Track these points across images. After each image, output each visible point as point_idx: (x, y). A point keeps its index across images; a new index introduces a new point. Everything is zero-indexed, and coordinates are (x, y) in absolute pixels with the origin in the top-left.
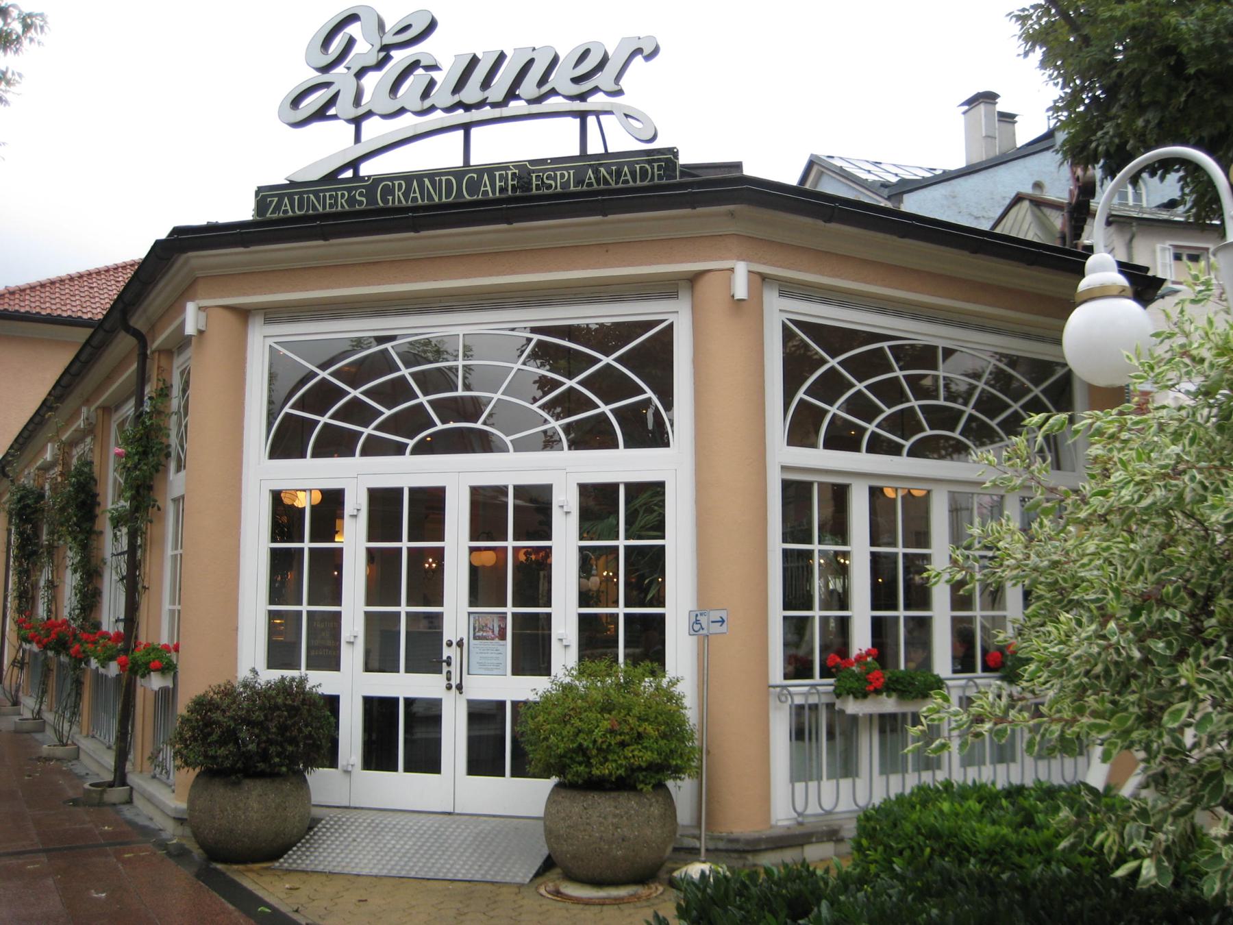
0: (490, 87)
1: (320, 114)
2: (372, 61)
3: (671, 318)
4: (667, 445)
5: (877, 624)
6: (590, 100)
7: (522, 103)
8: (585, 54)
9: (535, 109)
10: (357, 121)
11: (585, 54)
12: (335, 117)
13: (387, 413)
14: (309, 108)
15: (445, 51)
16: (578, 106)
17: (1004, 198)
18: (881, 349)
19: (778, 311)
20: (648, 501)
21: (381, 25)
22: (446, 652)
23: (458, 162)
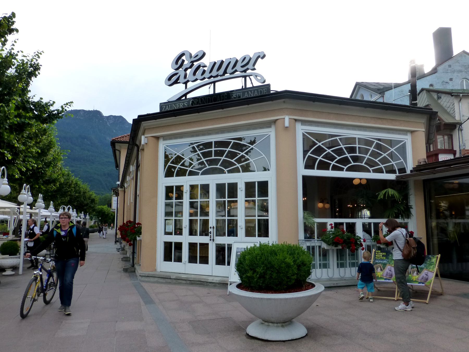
0: (223, 69)
1: (176, 82)
2: (188, 66)
3: (270, 133)
5: (191, 221)
6: (247, 72)
7: (228, 74)
8: (245, 58)
9: (223, 77)
10: (186, 83)
11: (245, 58)
12: (179, 83)
14: (173, 80)
15: (206, 61)
16: (244, 74)
18: (336, 139)
19: (301, 129)
21: (191, 55)
22: (210, 230)
23: (212, 92)
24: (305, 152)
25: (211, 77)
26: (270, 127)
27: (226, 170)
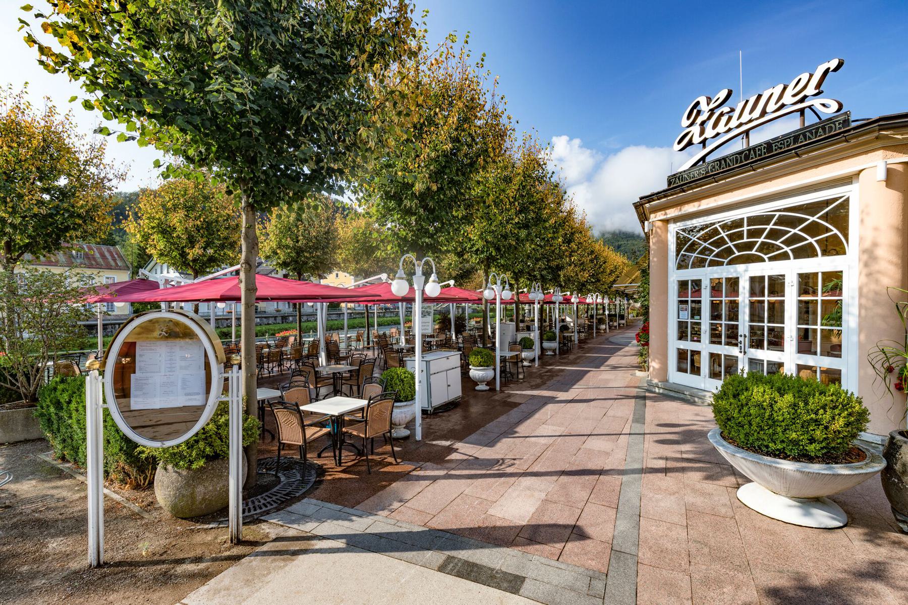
1: (690, 143)
4: (844, 253)
13: (717, 251)
17: (141, 356)
20: (834, 280)
22: (740, 339)
24: (678, 251)
25: (741, 125)
26: (851, 183)
27: (765, 257)
